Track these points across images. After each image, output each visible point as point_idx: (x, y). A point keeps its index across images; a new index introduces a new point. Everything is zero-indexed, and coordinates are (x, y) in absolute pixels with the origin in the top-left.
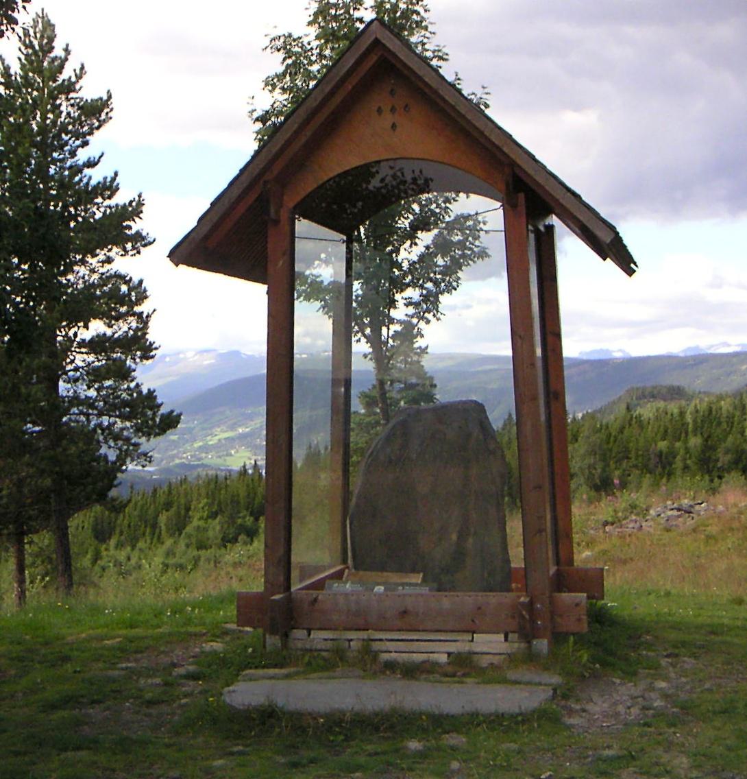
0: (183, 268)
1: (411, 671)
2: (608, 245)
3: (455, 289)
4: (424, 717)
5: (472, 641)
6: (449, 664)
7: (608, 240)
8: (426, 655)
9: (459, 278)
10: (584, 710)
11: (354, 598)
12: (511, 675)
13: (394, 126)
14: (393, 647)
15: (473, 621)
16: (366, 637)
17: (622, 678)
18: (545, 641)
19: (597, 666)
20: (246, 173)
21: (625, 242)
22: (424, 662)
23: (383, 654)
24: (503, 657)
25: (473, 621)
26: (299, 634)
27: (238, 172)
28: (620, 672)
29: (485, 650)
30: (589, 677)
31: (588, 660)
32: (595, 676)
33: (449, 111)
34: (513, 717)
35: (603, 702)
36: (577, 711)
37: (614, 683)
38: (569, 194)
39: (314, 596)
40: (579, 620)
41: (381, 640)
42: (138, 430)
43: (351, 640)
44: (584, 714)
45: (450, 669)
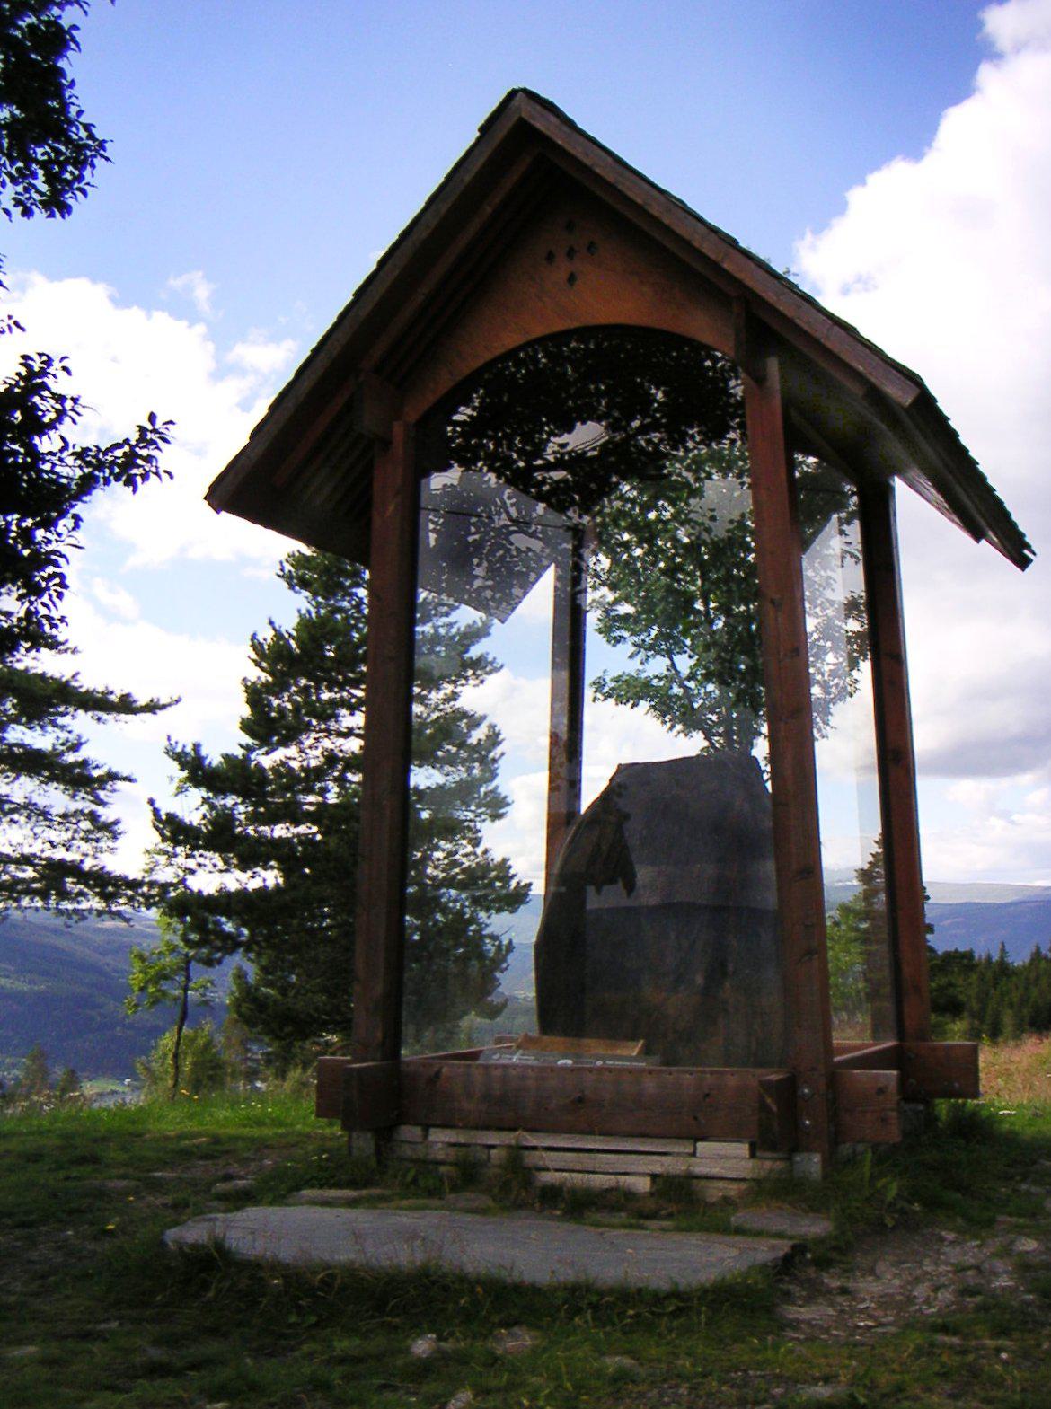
0: (225, 516)
1: (579, 1205)
2: (907, 410)
3: (851, 695)
4: (479, 1289)
5: (694, 1154)
6: (652, 1194)
7: (908, 400)
8: (612, 1177)
9: (856, 681)
10: (844, 1291)
11: (498, 1073)
12: (736, 1219)
13: (571, 279)
14: (562, 1161)
15: (695, 1118)
16: (513, 1142)
17: (959, 1232)
18: (817, 1158)
19: (917, 1207)
20: (322, 355)
21: (942, 405)
22: (610, 1190)
23: (543, 1173)
24: (744, 1186)
25: (695, 1118)
26: (410, 1132)
27: (309, 353)
28: (959, 1220)
29: (716, 1171)
30: (893, 1228)
31: (899, 1196)
32: (908, 1225)
33: (657, 237)
34: (658, 1299)
35: (895, 1275)
36: (829, 1291)
37: (942, 1239)
38: (836, 328)
39: (436, 1069)
40: (884, 1120)
41: (534, 1148)
42: (476, 901)
43: (493, 1147)
44: (840, 1299)
45: (651, 1205)
